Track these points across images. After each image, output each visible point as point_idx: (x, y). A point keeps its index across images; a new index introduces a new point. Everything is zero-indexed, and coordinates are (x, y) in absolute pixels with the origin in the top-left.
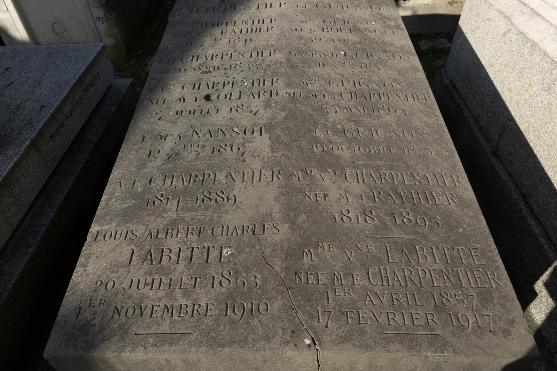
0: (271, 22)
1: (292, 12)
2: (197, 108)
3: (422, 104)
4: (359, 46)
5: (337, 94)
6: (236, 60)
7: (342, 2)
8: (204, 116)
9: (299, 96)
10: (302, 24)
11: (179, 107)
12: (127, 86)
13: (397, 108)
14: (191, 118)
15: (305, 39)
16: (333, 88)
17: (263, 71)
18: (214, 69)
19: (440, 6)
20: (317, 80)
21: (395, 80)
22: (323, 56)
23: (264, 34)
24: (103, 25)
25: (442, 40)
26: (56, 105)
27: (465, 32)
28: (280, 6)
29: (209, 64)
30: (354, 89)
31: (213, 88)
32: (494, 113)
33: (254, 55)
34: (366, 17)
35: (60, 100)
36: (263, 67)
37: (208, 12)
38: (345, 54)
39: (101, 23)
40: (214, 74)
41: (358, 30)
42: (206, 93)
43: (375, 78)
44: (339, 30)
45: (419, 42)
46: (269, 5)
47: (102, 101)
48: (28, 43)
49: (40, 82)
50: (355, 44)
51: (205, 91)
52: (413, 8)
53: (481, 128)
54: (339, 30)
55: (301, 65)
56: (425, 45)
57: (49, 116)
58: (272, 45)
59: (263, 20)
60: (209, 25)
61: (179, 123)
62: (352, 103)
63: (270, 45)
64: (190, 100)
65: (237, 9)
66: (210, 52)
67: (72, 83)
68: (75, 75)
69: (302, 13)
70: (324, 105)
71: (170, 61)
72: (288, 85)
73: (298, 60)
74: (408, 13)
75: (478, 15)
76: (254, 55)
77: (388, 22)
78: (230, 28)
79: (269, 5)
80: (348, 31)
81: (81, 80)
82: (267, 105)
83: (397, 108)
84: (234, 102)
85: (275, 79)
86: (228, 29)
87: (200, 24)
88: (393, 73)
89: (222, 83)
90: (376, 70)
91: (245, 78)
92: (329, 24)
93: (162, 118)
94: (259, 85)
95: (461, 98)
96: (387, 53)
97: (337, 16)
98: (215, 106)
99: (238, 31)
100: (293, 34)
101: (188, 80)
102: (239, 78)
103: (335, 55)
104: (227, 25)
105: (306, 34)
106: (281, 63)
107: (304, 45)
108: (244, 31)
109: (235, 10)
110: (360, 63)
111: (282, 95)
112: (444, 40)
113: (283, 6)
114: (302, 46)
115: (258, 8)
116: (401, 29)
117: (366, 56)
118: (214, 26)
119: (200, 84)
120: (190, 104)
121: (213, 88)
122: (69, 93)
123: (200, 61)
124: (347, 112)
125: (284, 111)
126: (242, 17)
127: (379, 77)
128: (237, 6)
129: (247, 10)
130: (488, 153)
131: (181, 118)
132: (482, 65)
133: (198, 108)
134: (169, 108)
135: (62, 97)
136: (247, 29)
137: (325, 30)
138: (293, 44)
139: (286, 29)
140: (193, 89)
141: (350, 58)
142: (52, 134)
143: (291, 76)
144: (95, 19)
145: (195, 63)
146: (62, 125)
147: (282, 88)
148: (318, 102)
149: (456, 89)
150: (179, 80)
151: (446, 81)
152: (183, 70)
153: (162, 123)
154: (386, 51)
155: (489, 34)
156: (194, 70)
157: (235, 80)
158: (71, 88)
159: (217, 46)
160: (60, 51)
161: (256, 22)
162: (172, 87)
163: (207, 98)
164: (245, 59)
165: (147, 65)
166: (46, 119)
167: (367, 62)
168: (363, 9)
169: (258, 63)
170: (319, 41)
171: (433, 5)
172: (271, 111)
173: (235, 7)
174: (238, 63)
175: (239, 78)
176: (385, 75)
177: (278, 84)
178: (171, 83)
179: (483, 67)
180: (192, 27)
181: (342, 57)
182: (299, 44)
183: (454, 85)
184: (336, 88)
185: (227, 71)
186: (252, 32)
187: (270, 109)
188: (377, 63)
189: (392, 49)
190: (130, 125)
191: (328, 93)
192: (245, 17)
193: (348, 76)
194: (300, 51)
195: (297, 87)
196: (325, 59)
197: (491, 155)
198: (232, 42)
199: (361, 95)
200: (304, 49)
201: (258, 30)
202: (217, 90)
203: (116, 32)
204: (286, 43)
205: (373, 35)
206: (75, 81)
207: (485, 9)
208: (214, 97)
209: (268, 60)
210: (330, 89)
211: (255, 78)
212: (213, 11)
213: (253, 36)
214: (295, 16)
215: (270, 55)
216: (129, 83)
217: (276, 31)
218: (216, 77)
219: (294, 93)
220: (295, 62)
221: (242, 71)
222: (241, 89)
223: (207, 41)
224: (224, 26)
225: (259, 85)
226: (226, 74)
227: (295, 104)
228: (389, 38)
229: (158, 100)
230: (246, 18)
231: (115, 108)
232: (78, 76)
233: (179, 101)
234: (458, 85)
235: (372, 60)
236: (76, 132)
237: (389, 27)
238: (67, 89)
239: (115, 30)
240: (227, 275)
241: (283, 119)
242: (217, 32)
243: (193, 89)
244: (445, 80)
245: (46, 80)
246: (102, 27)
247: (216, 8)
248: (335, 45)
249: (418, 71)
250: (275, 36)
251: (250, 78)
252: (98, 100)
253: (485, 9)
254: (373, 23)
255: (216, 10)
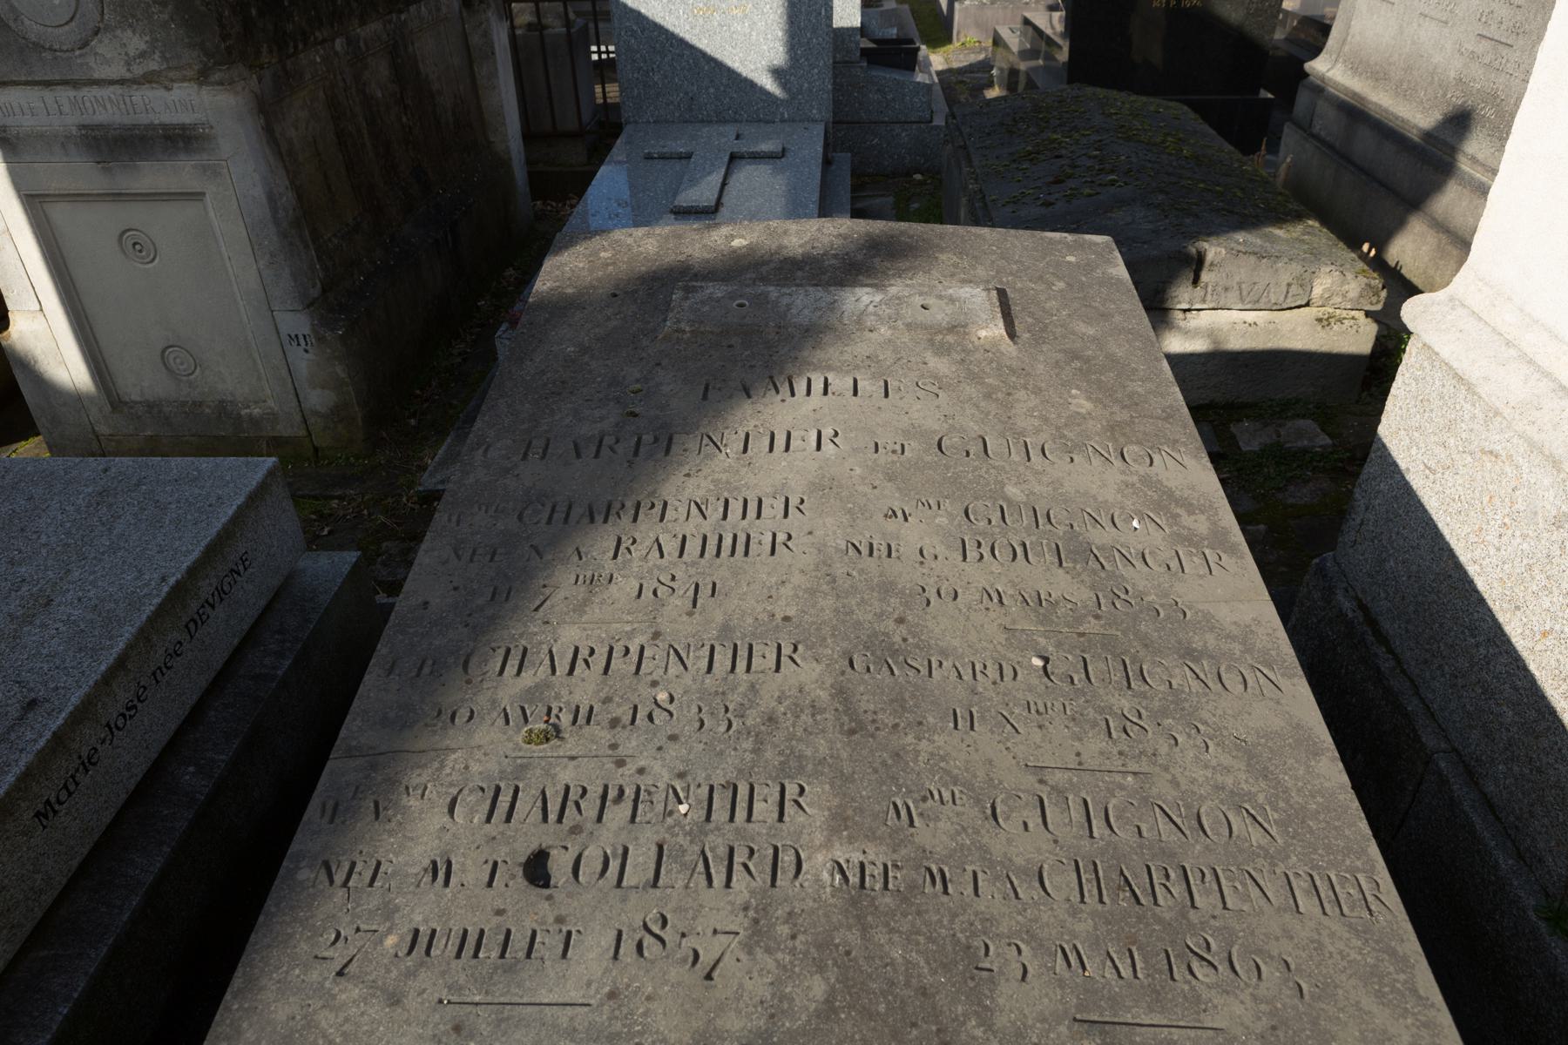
0: (786, 515)
1: (858, 471)
2: (491, 924)
3: (1357, 933)
4: (1091, 626)
5: (1024, 871)
6: (654, 684)
7: (1022, 434)
8: (510, 970)
9: (878, 886)
10: (891, 525)
11: (420, 912)
12: (339, 580)
13: (1260, 952)
14: (462, 979)
15: (902, 592)
16: (1009, 841)
17: (748, 744)
18: (575, 721)
19: (1293, 330)
20: (947, 795)
21: (1238, 800)
22: (967, 677)
23: (761, 568)
24: (307, 356)
25: (1301, 423)
26: (75, 700)
27: (1403, 465)
28: (819, 448)
29: (558, 697)
30: (1086, 842)
31: (560, 820)
32: (1539, 771)
33: (722, 660)
34: (1110, 494)
35: (96, 677)
36: (749, 722)
37: (578, 456)
38: (1045, 668)
39: (301, 349)
40: (571, 745)
41: (1087, 552)
42: (534, 846)
43: (1161, 789)
44: (1019, 550)
45: (1233, 429)
46: (780, 441)
47: (250, 638)
48: (90, 398)
49: (49, 602)
50: (1079, 620)
51: (528, 834)
52: (1211, 333)
53: (1489, 805)
54: (1019, 550)
55: (890, 721)
56: (1250, 438)
57: (42, 742)
58: (786, 619)
59: (760, 502)
60: (577, 511)
61: (412, 1002)
62: (1084, 926)
63: (779, 617)
64: (469, 879)
65: (674, 448)
66: (570, 636)
67: (148, 610)
68: (163, 579)
69: (891, 478)
70: (974, 934)
71: (426, 670)
72: (840, 824)
73: (883, 676)
74: (1198, 346)
75: (1449, 427)
76: (722, 660)
77: (1186, 520)
78: (647, 530)
79: (780, 441)
80: (1050, 558)
81: (179, 592)
82: (758, 934)
83: (1260, 952)
84: (633, 896)
85: (792, 790)
86: (637, 536)
87: (548, 509)
88: (1226, 760)
89: (595, 791)
90: (1164, 749)
91: (681, 775)
92: (983, 524)
93: (352, 968)
94: (732, 819)
95: (1403, 671)
96: (1197, 660)
97: (1011, 490)
98: (560, 920)
99: (670, 547)
100: (861, 571)
101: (475, 768)
102: (661, 774)
103: (1008, 672)
104: (635, 520)
105: (907, 574)
106: (815, 709)
107: (901, 621)
108: (693, 547)
109: (667, 451)
110: (1101, 711)
111: (818, 880)
112: (1307, 424)
113: (827, 446)
114: (891, 625)
115: (745, 450)
116: (1232, 550)
117: (1118, 676)
118: (592, 520)
119: (517, 790)
120: (466, 906)
121: (560, 820)
122: (130, 646)
123: (528, 679)
124: (1067, 975)
125: (821, 969)
126: (691, 482)
127: (1175, 783)
128: (676, 438)
129: (708, 456)
130: (1531, 913)
131: (423, 974)
132: (1477, 592)
133: (496, 920)
134: (389, 912)
135: (103, 668)
136: (705, 538)
137: (972, 554)
138: (860, 615)
139: (837, 550)
140: (488, 820)
141: (1066, 687)
142: (48, 802)
143: (849, 779)
144: (286, 340)
145: (511, 688)
146: (88, 763)
147: (819, 838)
148: (954, 916)
149: (1382, 639)
150: (442, 766)
151: (1347, 605)
152: (463, 714)
153: (349, 993)
154: (1189, 654)
155: (1496, 501)
156: (501, 721)
157: (644, 781)
158: (141, 630)
159: (594, 612)
160: (138, 484)
161: (736, 508)
162: (413, 802)
163: (537, 870)
164: (687, 679)
165: (424, 468)
166: (30, 757)
167: (1125, 704)
168: (1097, 461)
169: (734, 700)
170: (951, 604)
171: (1271, 327)
172: (770, 963)
173: (670, 440)
174: (662, 696)
175: (661, 774)
176: (1200, 774)
177: (801, 818)
178: (415, 780)
179: (1482, 601)
180: (520, 517)
181: (1035, 681)
182: (880, 616)
183: (1372, 622)
184: (1019, 842)
185: (621, 735)
186: (718, 554)
187: (768, 951)
188: (1164, 712)
189: (1211, 640)
190: (228, 996)
191: (992, 864)
192: (698, 487)
193: (1059, 778)
194: (887, 655)
195: (872, 837)
196: (974, 692)
197: (1542, 925)
198: (647, 594)
199: (1115, 876)
200: (897, 639)
201: (740, 548)
202: (576, 830)
203: (343, 375)
204: (836, 611)
205: (1136, 577)
206: (157, 601)
207: (1474, 417)
208: (560, 865)
209: (771, 687)
210: (997, 847)
211: (718, 779)
212: (597, 456)
213: (721, 571)
214: (868, 490)
215: (778, 669)
216: (346, 569)
217: (801, 556)
218: (575, 765)
219: (862, 866)
220: (866, 704)
221: (673, 738)
222: (664, 835)
223: (564, 584)
224: (626, 519)
225: (732, 819)
226: (614, 746)
227: (864, 929)
228: (1193, 590)
229: (353, 865)
230: (701, 492)
231: (287, 663)
232: (172, 581)
233: (428, 878)
234: (1387, 626)
235: (1144, 695)
236: (140, 770)
237: (1189, 539)
238: (128, 632)
239: (340, 370)
240: (656, 922)
241: (818, 1014)
242: (600, 543)
243: (488, 820)
244: (1340, 597)
245: (69, 596)
246: (304, 361)
247: (608, 440)
248: (1007, 621)
249: (1317, 753)
250: (797, 579)
251: (700, 779)
252: (236, 641)
253: (1474, 417)
254: (1135, 523)
255: (605, 451)
